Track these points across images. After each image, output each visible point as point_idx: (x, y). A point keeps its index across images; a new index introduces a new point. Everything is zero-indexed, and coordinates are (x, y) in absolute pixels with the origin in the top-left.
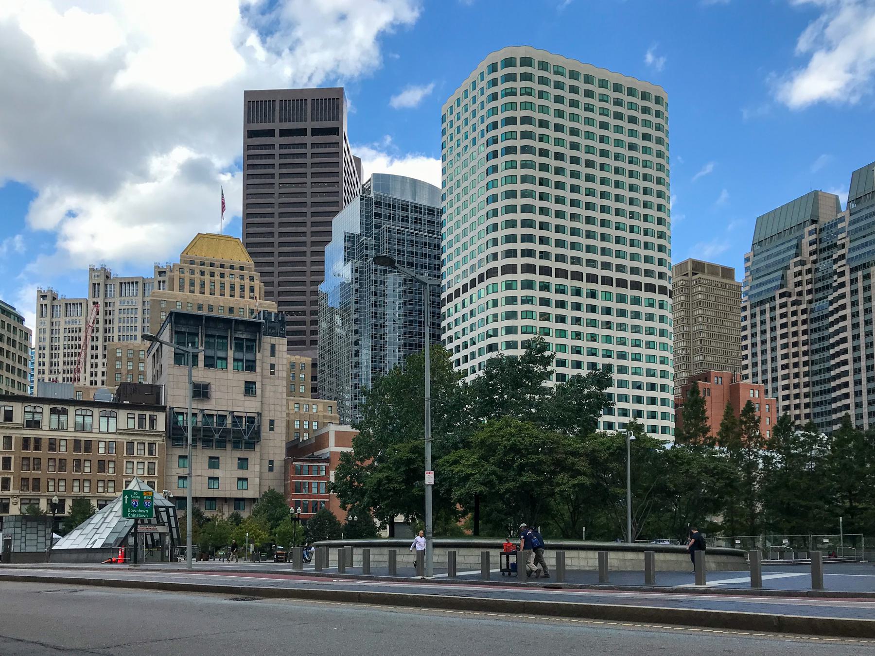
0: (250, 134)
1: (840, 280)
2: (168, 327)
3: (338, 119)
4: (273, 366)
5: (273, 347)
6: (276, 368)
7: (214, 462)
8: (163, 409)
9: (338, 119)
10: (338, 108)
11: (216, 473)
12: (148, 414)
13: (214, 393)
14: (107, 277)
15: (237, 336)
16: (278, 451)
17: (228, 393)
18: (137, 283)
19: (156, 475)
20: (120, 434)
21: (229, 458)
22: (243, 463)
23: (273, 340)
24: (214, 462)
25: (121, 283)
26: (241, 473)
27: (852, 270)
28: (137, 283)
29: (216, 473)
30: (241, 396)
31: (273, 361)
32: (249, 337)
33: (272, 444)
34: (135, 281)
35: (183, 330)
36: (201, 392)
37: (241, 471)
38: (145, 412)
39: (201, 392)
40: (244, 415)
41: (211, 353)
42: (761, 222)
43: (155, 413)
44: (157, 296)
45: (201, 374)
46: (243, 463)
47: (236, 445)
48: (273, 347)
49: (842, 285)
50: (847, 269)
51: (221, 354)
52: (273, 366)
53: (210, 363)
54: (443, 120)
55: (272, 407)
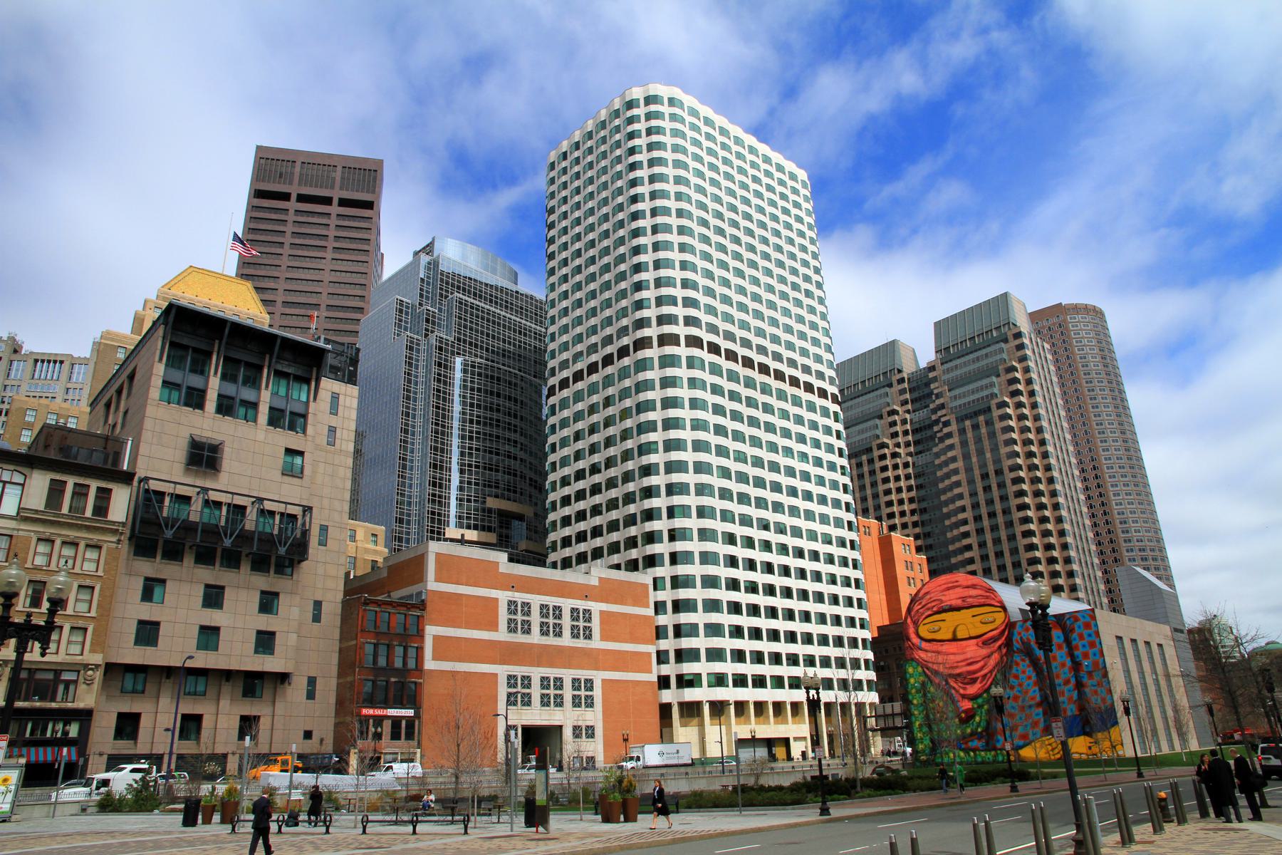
0: (258, 194)
1: (946, 430)
2: (161, 331)
3: (374, 192)
4: (332, 430)
5: (335, 397)
6: (338, 435)
7: (213, 597)
8: (127, 478)
9: (374, 192)
10: (375, 179)
11: (213, 617)
12: (94, 485)
13: (228, 462)
14: (15, 351)
15: (279, 367)
16: (330, 584)
17: (253, 464)
18: (62, 362)
19: (93, 614)
20: (26, 519)
21: (242, 590)
22: (268, 602)
23: (337, 386)
24: (213, 597)
25: (36, 361)
26: (265, 622)
27: (960, 420)
28: (62, 362)
29: (213, 617)
30: (277, 475)
31: (334, 421)
32: (299, 373)
33: (320, 571)
34: (59, 359)
35: (185, 341)
36: (204, 457)
37: (264, 617)
38: (87, 482)
39: (204, 457)
40: (281, 508)
41: (231, 389)
42: (941, 327)
43: (109, 486)
44: (112, 340)
45: (208, 424)
46: (268, 602)
47: (260, 564)
48: (335, 397)
49: (949, 435)
50: (952, 418)
51: (247, 394)
52: (332, 430)
53: (226, 406)
54: (552, 166)
55: (326, 502)
